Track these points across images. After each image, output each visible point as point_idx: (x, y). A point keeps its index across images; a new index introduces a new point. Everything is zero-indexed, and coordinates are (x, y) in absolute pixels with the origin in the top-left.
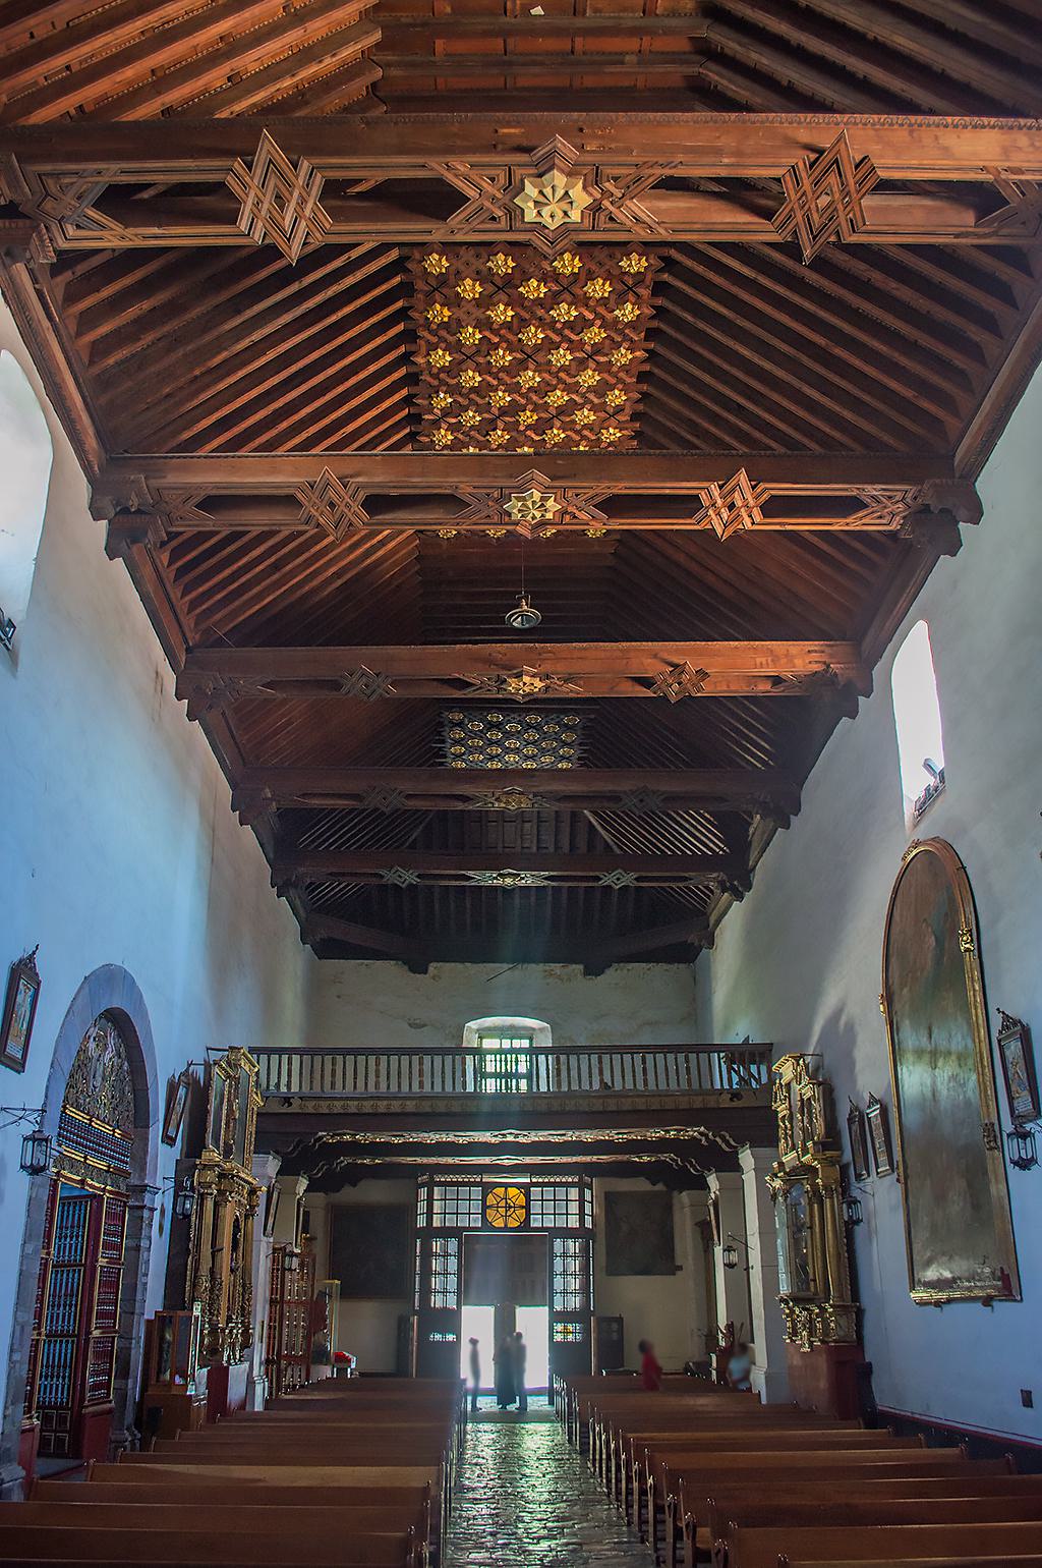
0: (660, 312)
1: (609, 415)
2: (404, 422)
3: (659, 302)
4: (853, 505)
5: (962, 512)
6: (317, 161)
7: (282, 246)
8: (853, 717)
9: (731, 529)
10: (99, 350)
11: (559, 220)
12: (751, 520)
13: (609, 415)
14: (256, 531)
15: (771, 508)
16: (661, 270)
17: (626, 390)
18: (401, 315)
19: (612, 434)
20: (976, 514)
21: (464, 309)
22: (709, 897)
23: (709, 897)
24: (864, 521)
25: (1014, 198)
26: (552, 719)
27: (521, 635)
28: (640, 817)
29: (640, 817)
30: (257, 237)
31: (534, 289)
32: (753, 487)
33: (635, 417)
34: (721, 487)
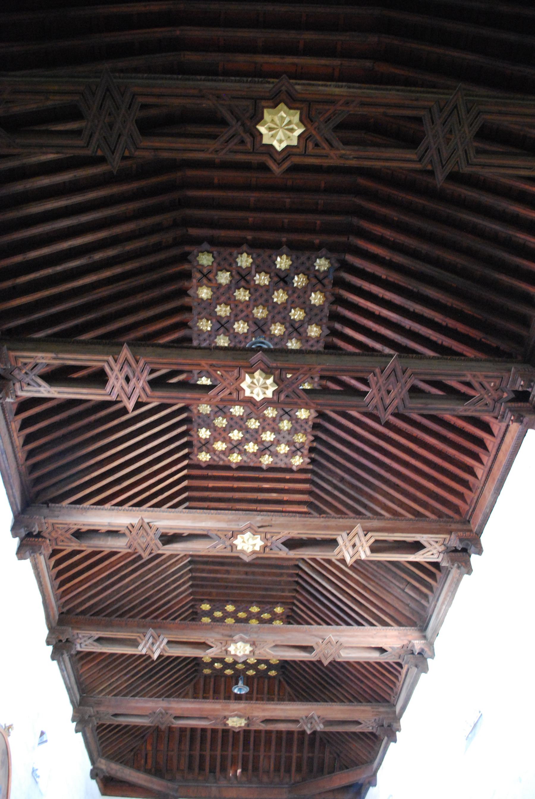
0: (317, 439)
1: (296, 450)
2: (188, 564)
3: (313, 456)
4: (417, 546)
5: (473, 548)
6: (149, 360)
7: (152, 655)
8: (433, 658)
9: (354, 559)
10: (65, 593)
11: (242, 653)
12: (365, 553)
13: (296, 450)
14: (107, 551)
15: (374, 549)
16: (337, 270)
17: (305, 433)
18: (185, 457)
19: (297, 461)
20: (480, 551)
21: (218, 432)
22: (461, 496)
23: (461, 496)
24: (425, 555)
25: (389, 650)
26: (267, 609)
27: (239, 698)
28: (388, 425)
29: (388, 425)
30: (144, 652)
31: (253, 424)
32: (365, 535)
33: (312, 450)
34: (348, 534)
